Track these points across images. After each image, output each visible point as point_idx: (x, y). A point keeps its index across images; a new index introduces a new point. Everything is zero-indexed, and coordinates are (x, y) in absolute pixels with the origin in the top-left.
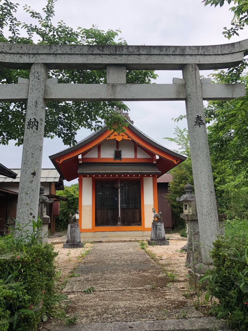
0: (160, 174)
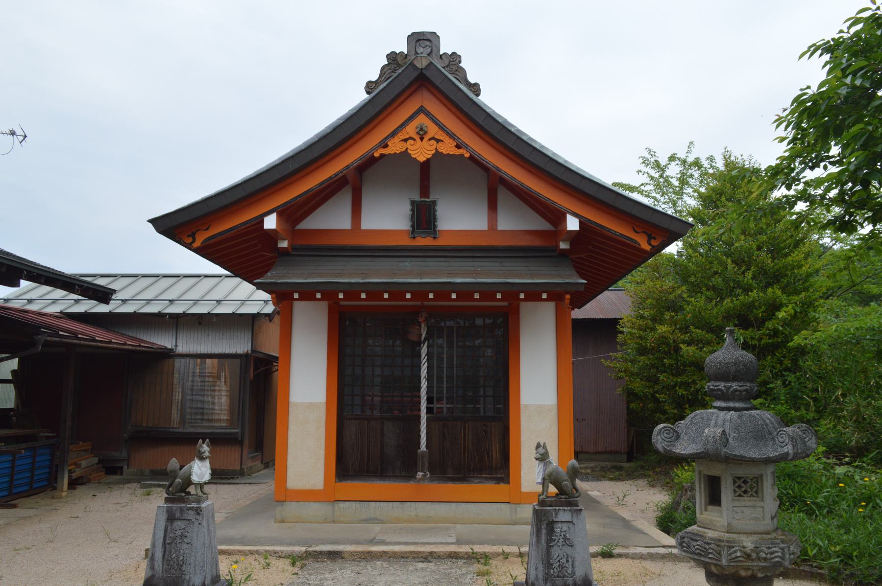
0: (582, 289)
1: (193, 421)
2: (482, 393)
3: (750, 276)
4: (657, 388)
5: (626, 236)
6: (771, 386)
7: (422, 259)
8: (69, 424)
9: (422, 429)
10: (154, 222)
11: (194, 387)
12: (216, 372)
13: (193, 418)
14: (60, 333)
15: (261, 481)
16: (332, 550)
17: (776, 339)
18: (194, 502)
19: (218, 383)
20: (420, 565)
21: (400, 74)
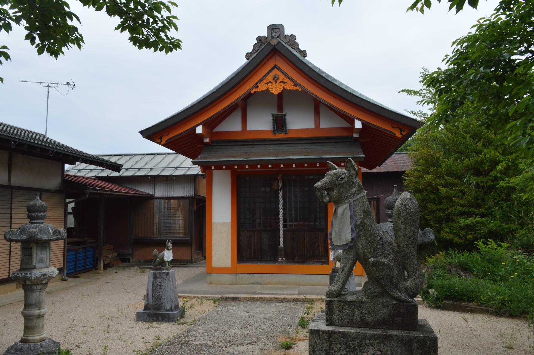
0: (363, 160)
1: (165, 233)
2: (318, 216)
3: (481, 145)
4: (426, 212)
5: (388, 130)
6: (492, 210)
7: (279, 145)
8: (102, 235)
9: (281, 236)
10: (142, 132)
11: (165, 215)
12: (176, 207)
13: (165, 231)
14: (97, 188)
15: (202, 266)
16: (234, 296)
17: (496, 182)
18: (166, 270)
19: (177, 213)
20: (278, 304)
21: (263, 49)
